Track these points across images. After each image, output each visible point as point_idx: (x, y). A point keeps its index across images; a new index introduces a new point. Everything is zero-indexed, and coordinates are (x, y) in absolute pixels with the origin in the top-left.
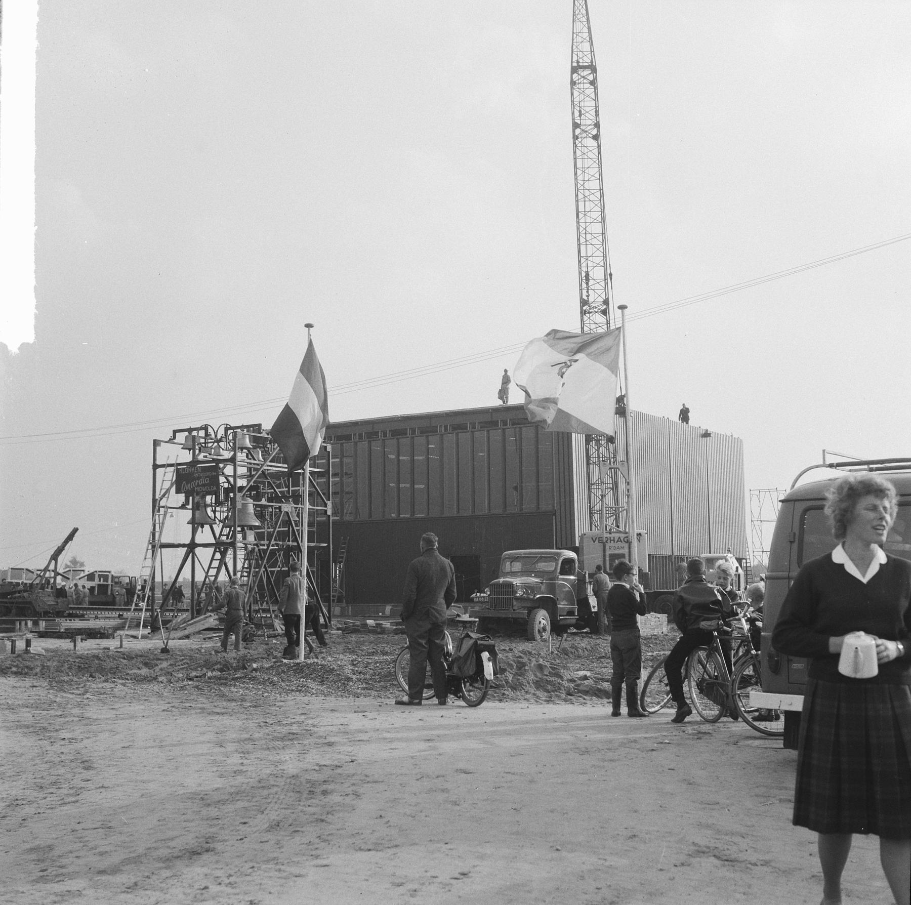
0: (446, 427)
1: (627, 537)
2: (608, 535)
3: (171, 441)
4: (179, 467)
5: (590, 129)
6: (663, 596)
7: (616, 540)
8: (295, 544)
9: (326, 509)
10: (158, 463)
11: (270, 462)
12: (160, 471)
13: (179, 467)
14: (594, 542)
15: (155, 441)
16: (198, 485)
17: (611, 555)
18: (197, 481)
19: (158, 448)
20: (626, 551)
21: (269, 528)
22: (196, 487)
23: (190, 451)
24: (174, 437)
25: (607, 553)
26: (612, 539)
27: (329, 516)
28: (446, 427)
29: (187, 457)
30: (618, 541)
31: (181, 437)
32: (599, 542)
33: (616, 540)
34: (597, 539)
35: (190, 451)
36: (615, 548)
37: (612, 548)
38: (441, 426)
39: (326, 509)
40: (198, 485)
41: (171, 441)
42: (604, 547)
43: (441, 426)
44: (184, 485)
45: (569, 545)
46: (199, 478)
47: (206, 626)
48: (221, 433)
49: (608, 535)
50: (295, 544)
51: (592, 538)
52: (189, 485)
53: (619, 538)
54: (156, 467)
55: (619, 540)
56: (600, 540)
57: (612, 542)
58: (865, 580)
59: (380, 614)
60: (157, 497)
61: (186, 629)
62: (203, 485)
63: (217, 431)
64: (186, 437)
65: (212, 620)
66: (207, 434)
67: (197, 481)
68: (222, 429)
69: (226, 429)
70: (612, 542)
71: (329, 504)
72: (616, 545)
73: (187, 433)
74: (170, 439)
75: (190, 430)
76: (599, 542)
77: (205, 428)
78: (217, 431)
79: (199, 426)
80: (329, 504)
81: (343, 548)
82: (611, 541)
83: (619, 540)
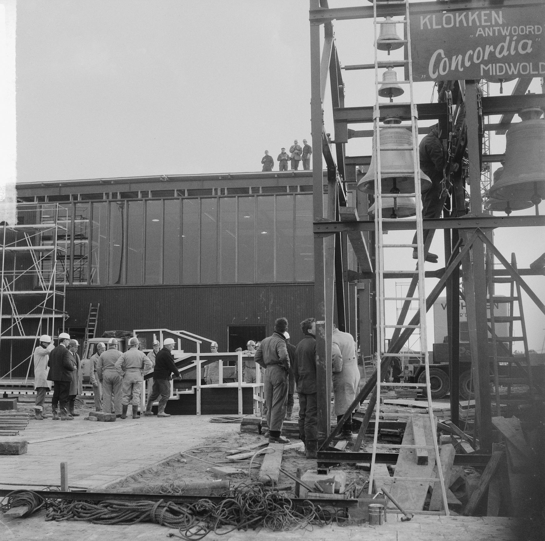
0: (222, 191)
16: (493, 59)
21: (5, 290)
22: (486, 63)
28: (222, 191)
40: (493, 59)
44: (439, 59)
52: (456, 61)
58: (135, 331)
81: (94, 316)
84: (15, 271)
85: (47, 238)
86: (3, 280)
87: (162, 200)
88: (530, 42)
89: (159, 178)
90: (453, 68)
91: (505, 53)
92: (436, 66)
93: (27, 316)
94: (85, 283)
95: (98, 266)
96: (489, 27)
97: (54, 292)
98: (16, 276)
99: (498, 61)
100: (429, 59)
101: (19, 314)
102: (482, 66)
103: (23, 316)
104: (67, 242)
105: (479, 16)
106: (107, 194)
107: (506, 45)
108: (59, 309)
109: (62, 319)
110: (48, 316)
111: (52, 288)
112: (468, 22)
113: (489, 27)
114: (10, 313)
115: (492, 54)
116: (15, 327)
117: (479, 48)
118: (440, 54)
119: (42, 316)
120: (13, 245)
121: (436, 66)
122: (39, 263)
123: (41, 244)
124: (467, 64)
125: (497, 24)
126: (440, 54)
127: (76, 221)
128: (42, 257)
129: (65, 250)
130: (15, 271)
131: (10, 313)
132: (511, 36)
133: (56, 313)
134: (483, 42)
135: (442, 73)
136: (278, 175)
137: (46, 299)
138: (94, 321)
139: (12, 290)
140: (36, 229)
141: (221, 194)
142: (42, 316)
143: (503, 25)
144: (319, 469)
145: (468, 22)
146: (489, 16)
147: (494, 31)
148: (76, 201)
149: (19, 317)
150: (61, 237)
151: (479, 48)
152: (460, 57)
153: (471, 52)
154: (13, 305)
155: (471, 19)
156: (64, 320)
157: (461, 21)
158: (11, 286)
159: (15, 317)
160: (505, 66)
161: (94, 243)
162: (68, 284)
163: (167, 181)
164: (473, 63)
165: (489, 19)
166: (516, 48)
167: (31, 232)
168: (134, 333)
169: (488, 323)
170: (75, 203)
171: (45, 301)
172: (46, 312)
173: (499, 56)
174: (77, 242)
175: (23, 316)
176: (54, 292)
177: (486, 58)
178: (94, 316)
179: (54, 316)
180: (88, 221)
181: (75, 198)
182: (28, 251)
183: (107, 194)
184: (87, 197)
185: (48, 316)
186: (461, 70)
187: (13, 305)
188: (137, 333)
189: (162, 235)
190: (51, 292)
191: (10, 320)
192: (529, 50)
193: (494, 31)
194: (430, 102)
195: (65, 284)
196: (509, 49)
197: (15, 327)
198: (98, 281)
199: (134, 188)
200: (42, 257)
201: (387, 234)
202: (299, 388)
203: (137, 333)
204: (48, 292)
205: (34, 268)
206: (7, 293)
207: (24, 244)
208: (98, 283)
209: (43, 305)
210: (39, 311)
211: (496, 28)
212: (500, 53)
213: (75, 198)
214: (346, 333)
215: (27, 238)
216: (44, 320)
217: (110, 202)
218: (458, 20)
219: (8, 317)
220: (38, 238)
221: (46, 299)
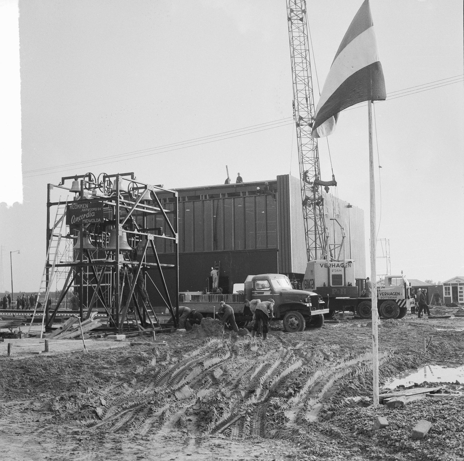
0: (206, 196)
1: (343, 264)
2: (331, 263)
3: (59, 186)
4: (69, 204)
5: (294, 16)
6: (364, 302)
8: (156, 264)
9: (174, 239)
10: (51, 201)
11: (139, 203)
12: (52, 208)
13: (69, 204)
14: (322, 267)
15: (49, 185)
16: (85, 218)
17: (333, 276)
18: (85, 215)
19: (51, 191)
22: (84, 219)
23: (76, 193)
24: (63, 183)
25: (331, 273)
26: (334, 265)
27: (177, 244)
28: (206, 196)
29: (71, 197)
30: (337, 266)
31: (69, 184)
32: (325, 267)
34: (324, 265)
35: (76, 193)
37: (334, 271)
38: (202, 196)
39: (174, 239)
40: (85, 218)
41: (59, 186)
43: (202, 196)
44: (73, 218)
45: (284, 272)
46: (86, 212)
47: (94, 327)
48: (101, 179)
49: (331, 263)
50: (156, 264)
51: (320, 264)
53: (338, 264)
54: (49, 204)
55: (338, 266)
56: (326, 266)
57: (334, 267)
59: (162, 313)
60: (51, 227)
61: (77, 330)
62: (89, 218)
63: (98, 178)
64: (73, 183)
65: (97, 322)
66: (90, 180)
67: (85, 215)
68: (102, 175)
69: (104, 177)
70: (334, 267)
71: (177, 235)
73: (74, 180)
74: (59, 185)
75: (76, 178)
76: (325, 267)
77: (89, 175)
78: (98, 178)
79: (84, 174)
80: (177, 235)
82: (332, 266)
83: (338, 266)
91: (88, 216)
92: (73, 221)
99: (87, 218)
115: (85, 216)
121: (73, 221)
124: (80, 220)
125: (87, 208)
132: (90, 211)
134: (84, 213)
136: (236, 185)
141: (205, 198)
143: (88, 208)
144: (323, 315)
146: (85, 205)
148: (166, 203)
160: (88, 220)
163: (210, 189)
165: (85, 207)
169: (235, 292)
194: (222, 183)
198: (84, 261)
202: (61, 371)
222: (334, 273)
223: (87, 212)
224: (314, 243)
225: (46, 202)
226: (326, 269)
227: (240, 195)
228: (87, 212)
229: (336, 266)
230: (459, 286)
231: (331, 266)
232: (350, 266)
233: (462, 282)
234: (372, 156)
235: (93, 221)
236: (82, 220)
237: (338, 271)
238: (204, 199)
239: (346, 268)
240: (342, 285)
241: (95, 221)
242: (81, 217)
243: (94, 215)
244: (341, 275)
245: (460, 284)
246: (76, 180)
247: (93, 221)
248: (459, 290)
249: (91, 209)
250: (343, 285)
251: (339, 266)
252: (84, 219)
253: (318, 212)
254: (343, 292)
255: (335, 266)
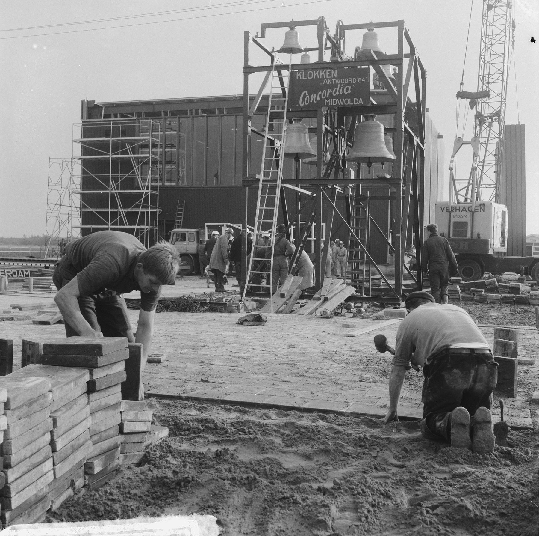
7: (461, 209)
10: (251, 63)
14: (442, 211)
16: (331, 96)
17: (455, 223)
18: (329, 91)
20: (468, 220)
21: (112, 190)
22: (327, 98)
25: (453, 220)
30: (463, 210)
33: (461, 209)
36: (459, 216)
37: (456, 217)
40: (331, 96)
42: (450, 215)
44: (305, 96)
52: (313, 96)
53: (464, 207)
57: (458, 211)
58: (206, 224)
64: (287, 34)
70: (458, 211)
72: (461, 214)
73: (287, 29)
81: (181, 210)
82: (456, 210)
84: (120, 174)
85: (145, 146)
86: (111, 182)
87: (234, 117)
88: (350, 87)
89: (232, 97)
90: (311, 101)
91: (337, 93)
92: (303, 100)
93: (129, 210)
94: (174, 184)
95: (185, 169)
96: (330, 79)
97: (150, 192)
98: (121, 178)
99: (334, 97)
100: (300, 96)
101: (124, 208)
102: (326, 100)
103: (126, 210)
104: (159, 150)
105: (325, 73)
106: (191, 111)
107: (338, 89)
108: (154, 206)
109: (156, 212)
110: (145, 210)
111: (148, 189)
112: (320, 77)
113: (330, 79)
114: (117, 208)
115: (331, 94)
116: (121, 218)
117: (325, 91)
118: (305, 93)
119: (140, 210)
120: (118, 154)
121: (303, 100)
122: (138, 168)
123: (140, 153)
124: (318, 99)
125: (334, 78)
126: (305, 93)
127: (167, 133)
128: (141, 162)
129: (158, 158)
130: (120, 174)
131: (117, 208)
132: (341, 84)
133: (151, 208)
135: (306, 104)
137: (143, 197)
138: (181, 214)
139: (118, 190)
140: (135, 140)
142: (140, 210)
143: (337, 78)
145: (320, 77)
146: (330, 72)
147: (332, 81)
149: (123, 210)
150: (154, 146)
151: (325, 91)
152: (315, 95)
153: (320, 92)
154: (119, 202)
155: (321, 74)
156: (158, 213)
157: (316, 75)
158: (117, 186)
159: (121, 210)
160: (337, 100)
161: (181, 151)
162: (161, 184)
163: (187, 103)
164: (321, 98)
165: (330, 75)
166: (343, 91)
167: (131, 143)
168: (205, 226)
170: (166, 119)
171: (143, 199)
172: (143, 207)
173: (334, 95)
174: (167, 150)
175: (126, 210)
176: (150, 192)
177: (328, 96)
178: (181, 210)
179: (149, 210)
180: (175, 133)
181: (166, 114)
182: (130, 158)
183: (191, 111)
184: (174, 114)
185: (145, 210)
186: (315, 102)
187: (119, 202)
188: (207, 226)
189: (234, 147)
190: (147, 191)
191: (117, 213)
192: (349, 92)
193: (332, 81)
195: (159, 184)
196: (339, 91)
197: (121, 218)
199: (212, 106)
200: (141, 162)
201: (524, 125)
203: (207, 226)
204: (145, 191)
205: (134, 172)
206: (114, 191)
207: (126, 152)
208: (185, 184)
209: (141, 202)
210: (138, 206)
211: (333, 80)
212: (335, 93)
213: (166, 114)
214: (134, 237)
215: (128, 147)
216: (142, 213)
217: (193, 117)
218: (315, 74)
219: (116, 210)
220: (137, 147)
221: (143, 197)
222: (457, 220)
223: (335, 85)
224: (484, 171)
225: (242, 65)
226: (447, 214)
227: (215, 113)
228: (335, 85)
229: (461, 210)
230: (533, 247)
231: (454, 211)
232: (484, 211)
233: (537, 241)
234: (409, 67)
235: (347, 101)
236: (324, 100)
237: (462, 217)
238: (194, 115)
239: (475, 214)
240: (466, 236)
241: (352, 102)
242: (320, 95)
243: (349, 92)
244: (465, 224)
245: (535, 244)
246: (292, 29)
247: (347, 101)
248: (533, 251)
249: (345, 80)
250: (469, 236)
251: (466, 210)
252: (327, 98)
253: (77, 161)
254: (464, 247)
255: (459, 209)
